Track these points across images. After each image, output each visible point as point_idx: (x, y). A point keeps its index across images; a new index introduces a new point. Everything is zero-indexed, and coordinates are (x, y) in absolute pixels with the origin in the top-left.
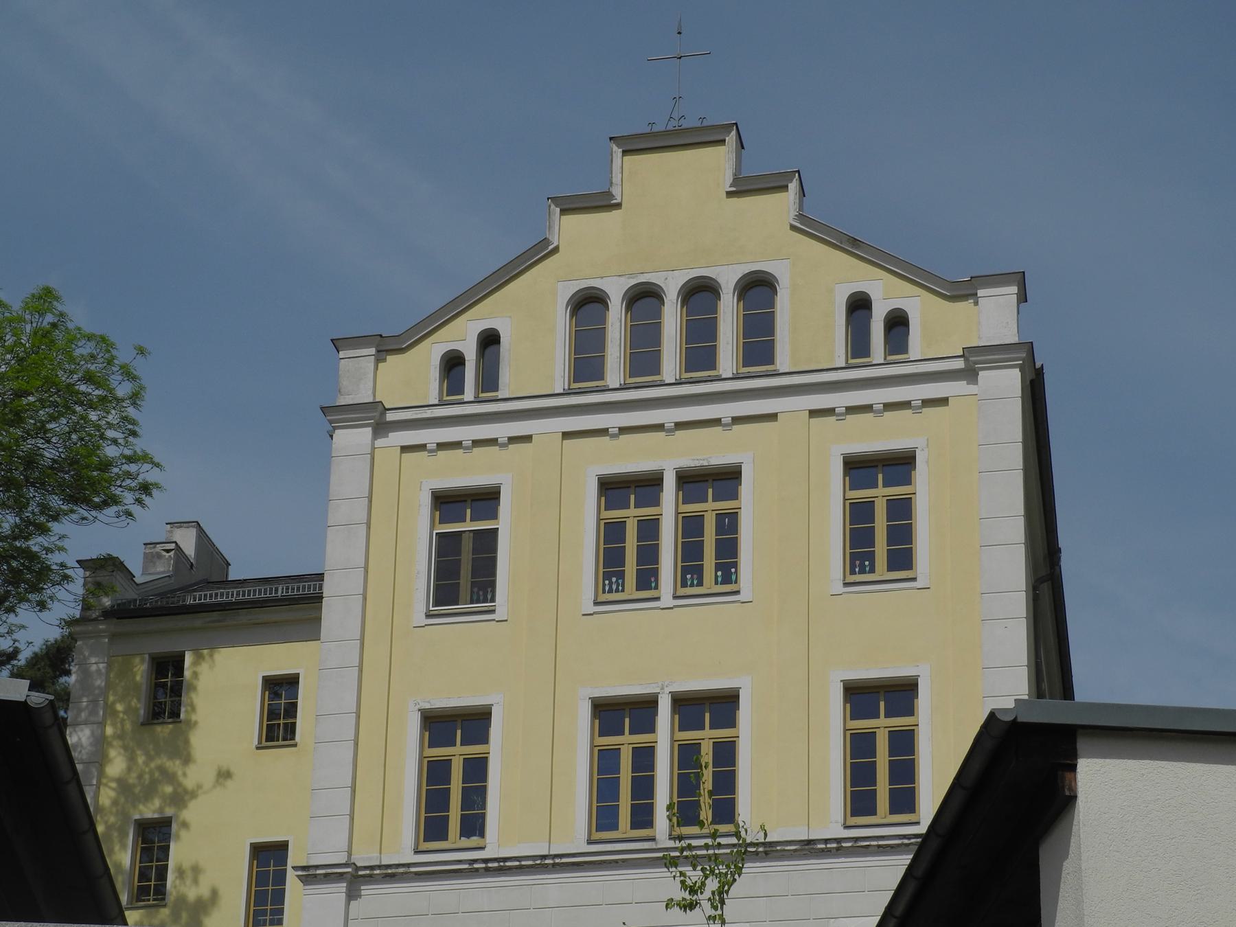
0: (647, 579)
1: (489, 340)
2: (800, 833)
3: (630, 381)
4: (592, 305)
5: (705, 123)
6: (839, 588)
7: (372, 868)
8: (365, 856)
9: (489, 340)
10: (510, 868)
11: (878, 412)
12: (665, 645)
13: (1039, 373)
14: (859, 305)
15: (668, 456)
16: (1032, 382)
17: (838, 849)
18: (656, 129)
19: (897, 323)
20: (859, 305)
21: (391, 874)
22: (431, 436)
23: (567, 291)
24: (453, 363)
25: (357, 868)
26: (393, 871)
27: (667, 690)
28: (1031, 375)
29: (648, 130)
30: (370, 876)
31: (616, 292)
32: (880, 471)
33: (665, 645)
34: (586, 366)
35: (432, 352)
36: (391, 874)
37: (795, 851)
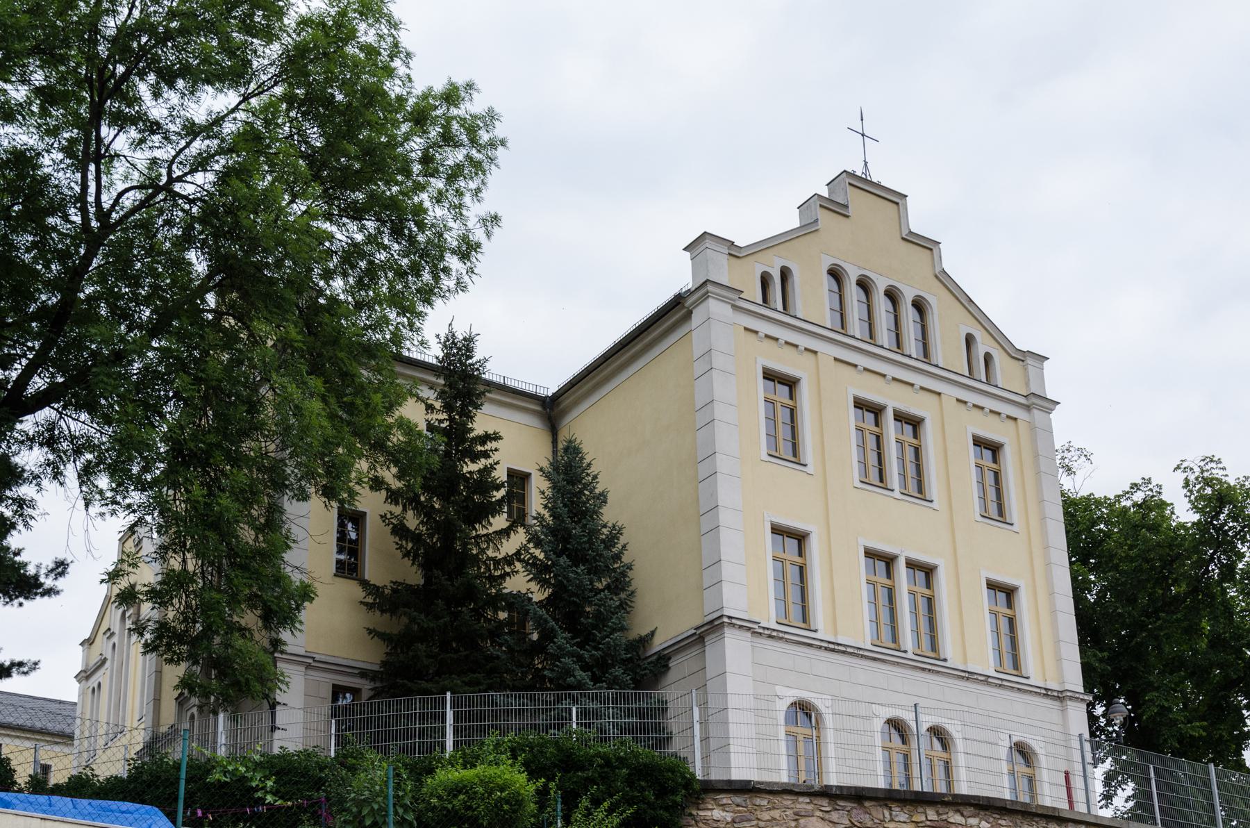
10: (787, 640)
14: (970, 340)
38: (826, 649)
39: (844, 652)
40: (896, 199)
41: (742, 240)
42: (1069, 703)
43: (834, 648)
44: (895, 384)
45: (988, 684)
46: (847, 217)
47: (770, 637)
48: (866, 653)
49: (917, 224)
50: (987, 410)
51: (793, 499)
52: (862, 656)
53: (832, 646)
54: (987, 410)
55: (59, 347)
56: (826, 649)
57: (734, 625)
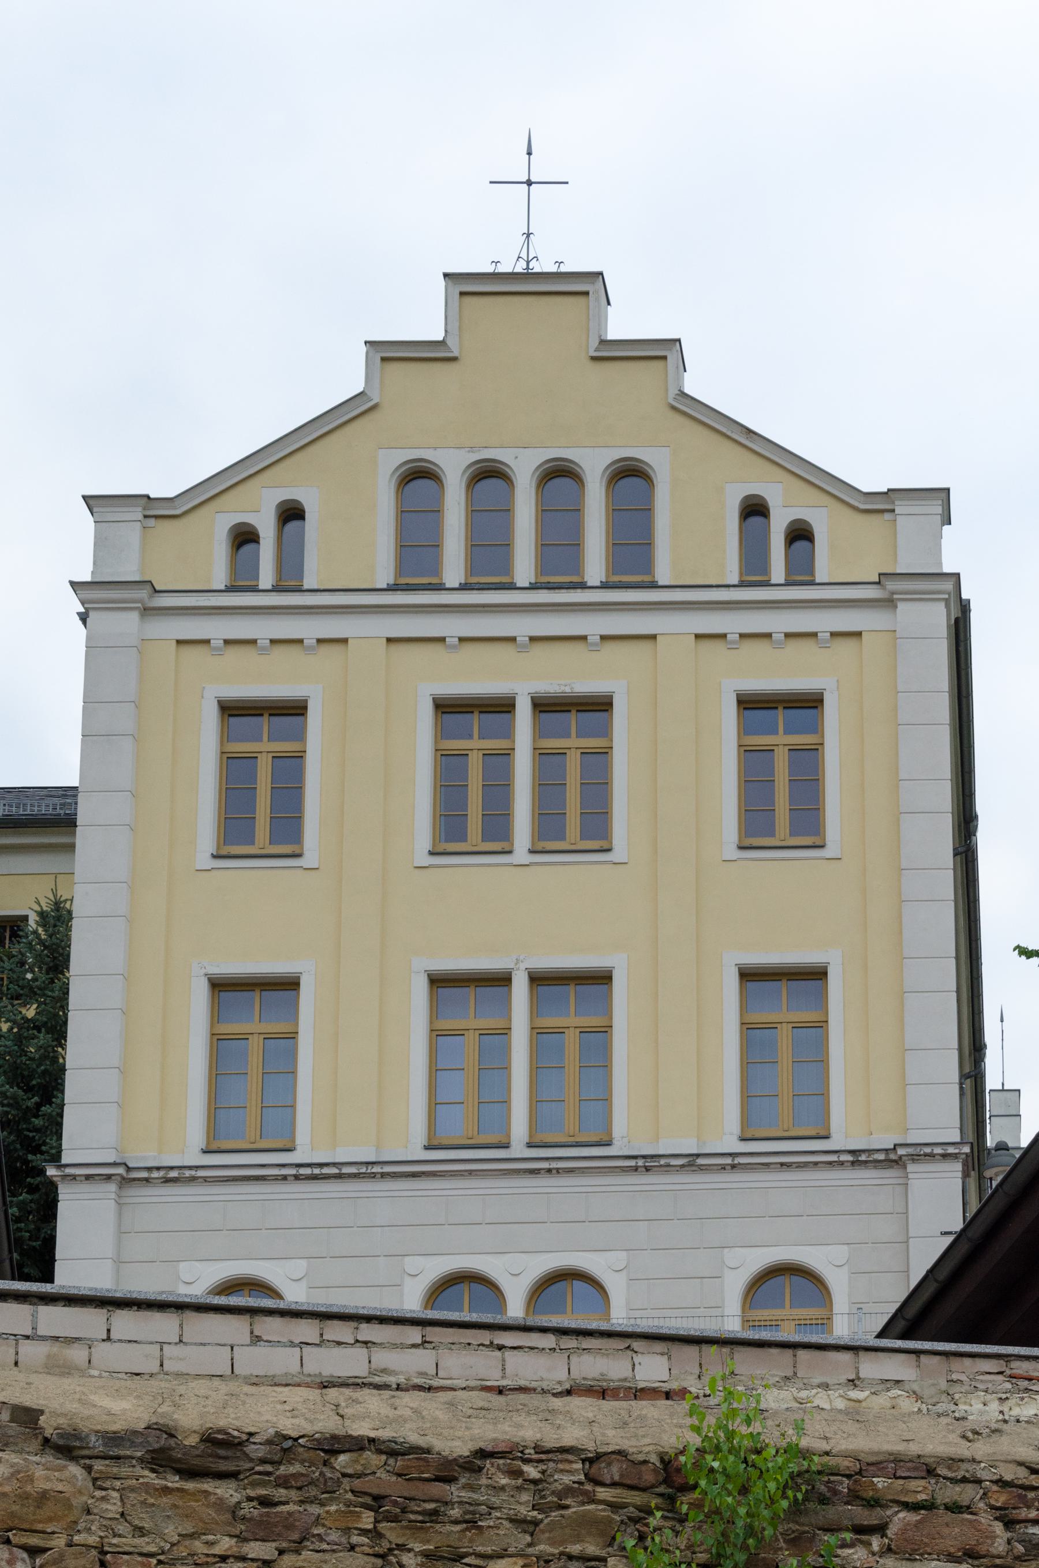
0: (498, 829)
1: (291, 514)
2: (690, 1147)
3: (474, 580)
4: (635, 479)
5: (563, 269)
6: (730, 851)
7: (149, 1169)
8: (144, 1154)
9: (291, 514)
10: (205, 1180)
11: (311, 648)
12: (522, 911)
13: (965, 608)
14: (754, 510)
15: (524, 679)
16: (957, 620)
17: (853, 1163)
18: (501, 269)
19: (800, 534)
20: (754, 510)
21: (173, 1177)
22: (217, 629)
23: (391, 462)
24: (244, 537)
25: (129, 1169)
26: (193, 1173)
27: (522, 966)
28: (955, 613)
29: (490, 269)
30: (147, 1180)
31: (594, 468)
32: (265, 721)
33: (522, 911)
34: (416, 560)
35: (220, 524)
36: (173, 1177)
37: (683, 1166)
38: (297, 1177)
39: (339, 1176)
40: (583, 288)
41: (165, 485)
42: (911, 1167)
43: (648, 1164)
44: (538, 649)
45: (703, 1168)
46: (454, 359)
47: (167, 1181)
48: (387, 1169)
49: (623, 323)
50: (778, 637)
51: (257, 919)
52: (383, 1175)
53: (307, 1171)
54: (778, 637)
55: (43, 951)
56: (297, 1177)
57: (74, 1177)
